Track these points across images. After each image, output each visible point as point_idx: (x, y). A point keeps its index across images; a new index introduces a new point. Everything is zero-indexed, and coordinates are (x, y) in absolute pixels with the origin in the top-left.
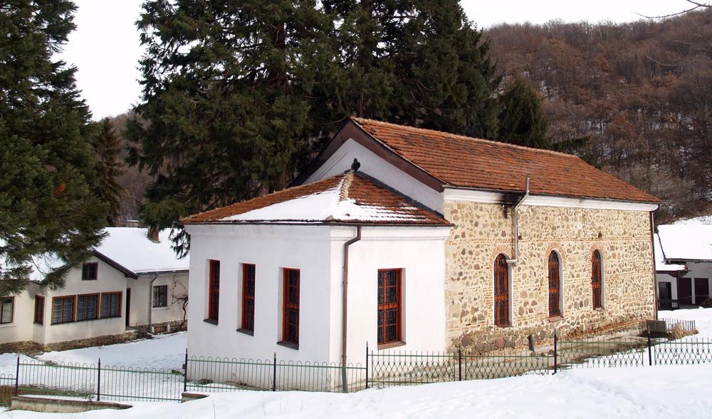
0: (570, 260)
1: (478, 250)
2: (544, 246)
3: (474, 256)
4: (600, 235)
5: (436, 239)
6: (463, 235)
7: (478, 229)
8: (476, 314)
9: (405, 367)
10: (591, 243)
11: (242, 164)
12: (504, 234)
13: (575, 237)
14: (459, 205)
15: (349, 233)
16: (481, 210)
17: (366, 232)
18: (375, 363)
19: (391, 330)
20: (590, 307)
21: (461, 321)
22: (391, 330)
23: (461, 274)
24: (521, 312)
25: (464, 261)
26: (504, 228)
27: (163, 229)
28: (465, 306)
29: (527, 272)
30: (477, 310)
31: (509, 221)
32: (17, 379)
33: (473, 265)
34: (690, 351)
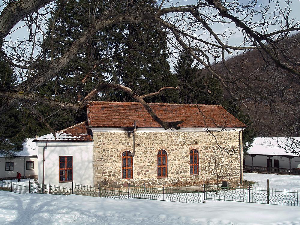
0: (172, 153)
1: (112, 150)
2: (155, 148)
3: (109, 152)
4: (196, 143)
5: (90, 146)
6: (104, 144)
7: (112, 142)
8: (111, 174)
9: (196, 197)
10: (189, 147)
11: (30, 80)
12: (128, 144)
13: (177, 144)
14: (101, 133)
15: (45, 144)
16: (114, 134)
17: (49, 144)
18: (254, 194)
19: (162, 172)
20: (188, 174)
21: (102, 176)
22: (162, 172)
23: (102, 158)
24: (139, 174)
25: (104, 154)
26: (128, 141)
27: (3, 52)
28: (105, 170)
29: (143, 159)
30: (112, 172)
31: (132, 138)
32: (72, 190)
33: (109, 155)
34: (274, 195)
